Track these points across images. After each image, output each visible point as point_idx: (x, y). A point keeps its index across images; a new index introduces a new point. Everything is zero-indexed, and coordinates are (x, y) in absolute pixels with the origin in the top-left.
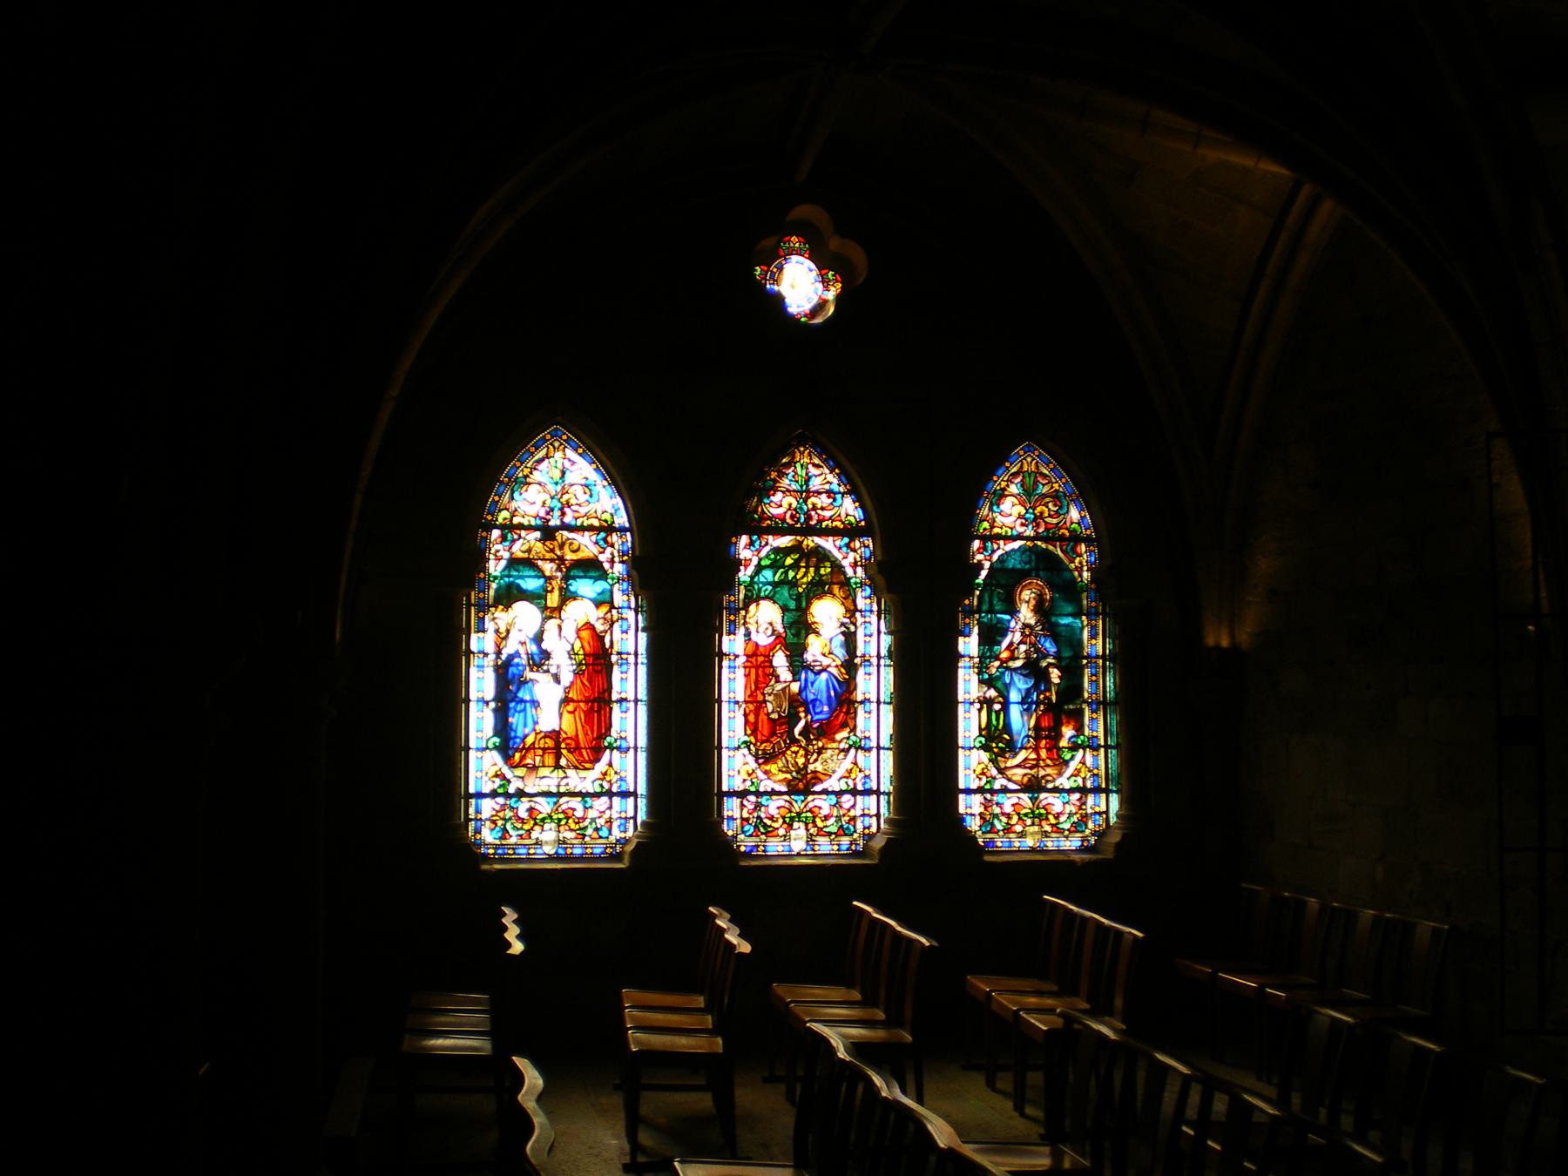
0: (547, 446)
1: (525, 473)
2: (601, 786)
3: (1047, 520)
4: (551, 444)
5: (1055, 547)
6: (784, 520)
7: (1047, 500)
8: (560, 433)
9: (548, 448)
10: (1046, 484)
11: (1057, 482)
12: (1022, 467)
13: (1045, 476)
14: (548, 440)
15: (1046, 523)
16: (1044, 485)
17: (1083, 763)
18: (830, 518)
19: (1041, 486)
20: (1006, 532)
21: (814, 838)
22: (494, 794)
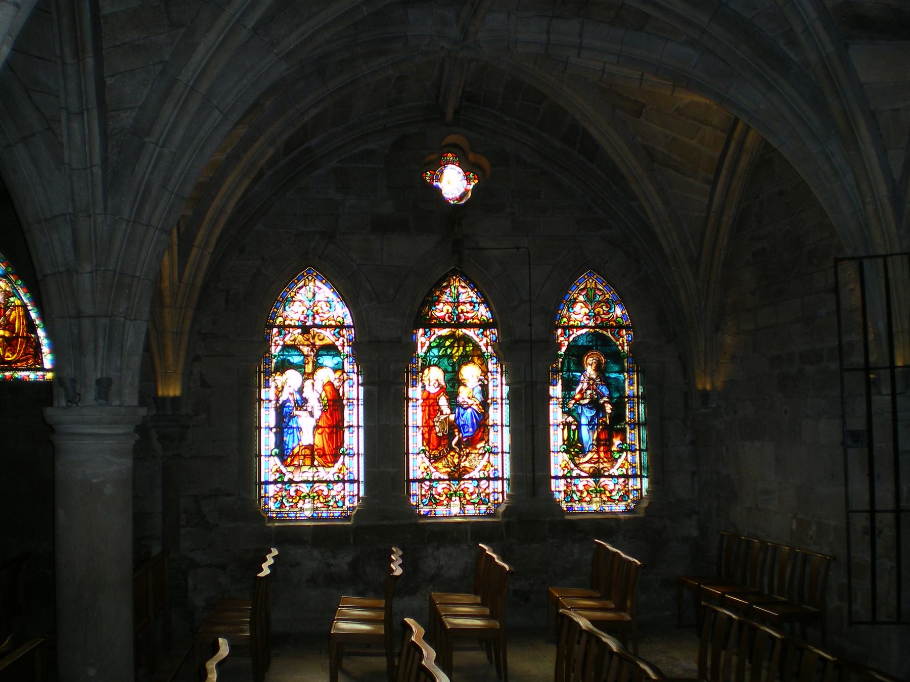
0: (304, 279)
1: (292, 295)
2: (338, 476)
3: (602, 316)
4: (307, 278)
5: (607, 332)
6: (444, 320)
7: (602, 304)
8: (312, 272)
9: (305, 280)
10: (601, 295)
11: (608, 294)
12: (586, 285)
13: (600, 290)
14: (305, 276)
15: (601, 318)
16: (600, 296)
17: (626, 460)
18: (472, 318)
19: (598, 296)
20: (577, 324)
21: (464, 506)
22: (275, 482)
